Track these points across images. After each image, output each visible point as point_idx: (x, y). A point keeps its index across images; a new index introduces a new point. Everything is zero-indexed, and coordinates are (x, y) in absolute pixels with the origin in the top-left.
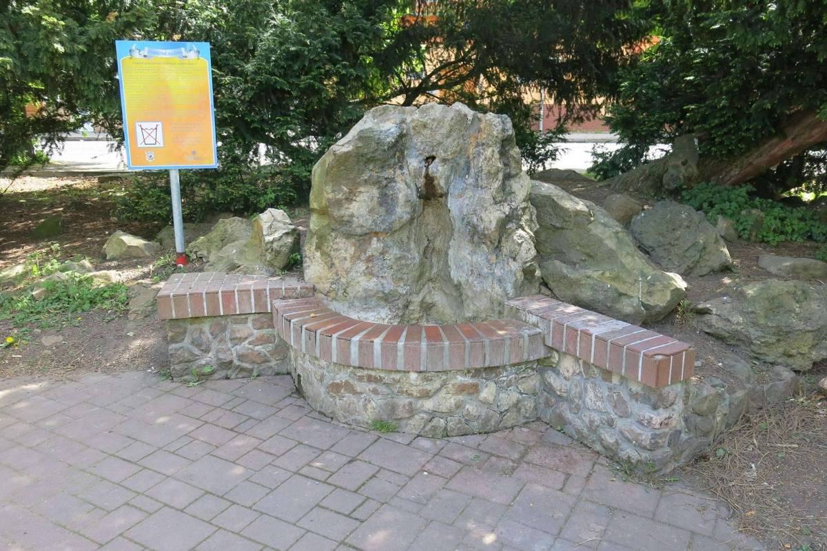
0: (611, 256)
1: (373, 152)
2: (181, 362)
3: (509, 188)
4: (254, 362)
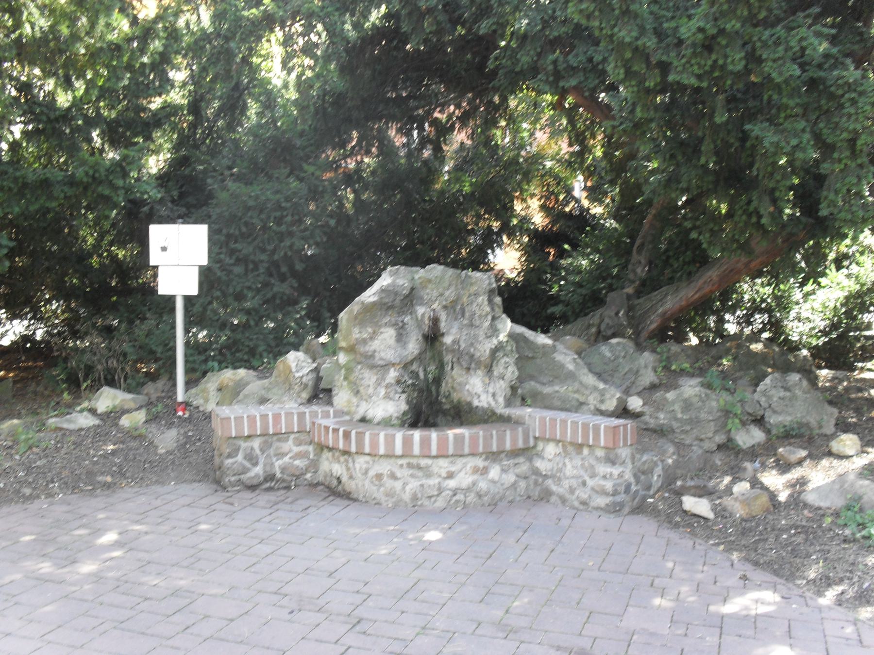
0: (571, 376)
2: (234, 475)
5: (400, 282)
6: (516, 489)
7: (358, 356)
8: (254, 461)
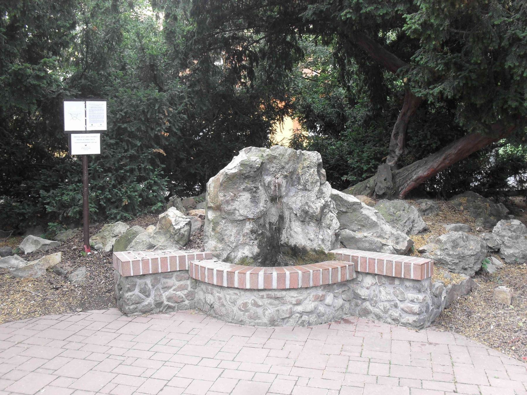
0: (374, 225)
1: (248, 173)
2: (133, 304)
4: (176, 302)
6: (343, 309)
7: (223, 213)
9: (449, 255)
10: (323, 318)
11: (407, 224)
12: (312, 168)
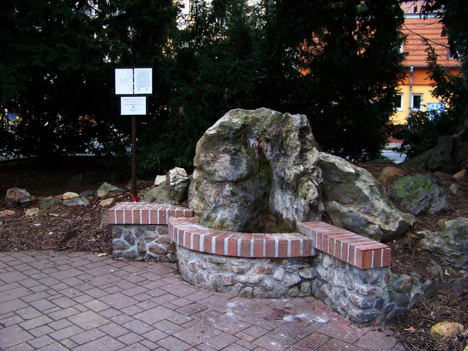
0: (365, 199)
1: (227, 135)
2: (118, 249)
3: (305, 157)
4: (157, 253)
5: (235, 120)
8: (131, 241)
9: (449, 244)
10: (271, 292)
11: (422, 203)
12: (292, 132)
